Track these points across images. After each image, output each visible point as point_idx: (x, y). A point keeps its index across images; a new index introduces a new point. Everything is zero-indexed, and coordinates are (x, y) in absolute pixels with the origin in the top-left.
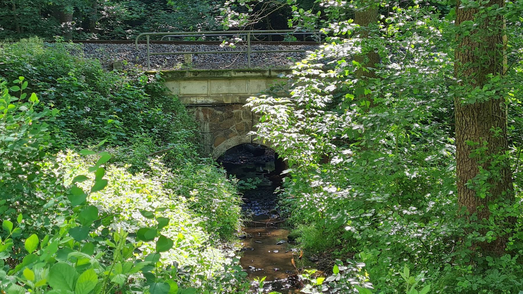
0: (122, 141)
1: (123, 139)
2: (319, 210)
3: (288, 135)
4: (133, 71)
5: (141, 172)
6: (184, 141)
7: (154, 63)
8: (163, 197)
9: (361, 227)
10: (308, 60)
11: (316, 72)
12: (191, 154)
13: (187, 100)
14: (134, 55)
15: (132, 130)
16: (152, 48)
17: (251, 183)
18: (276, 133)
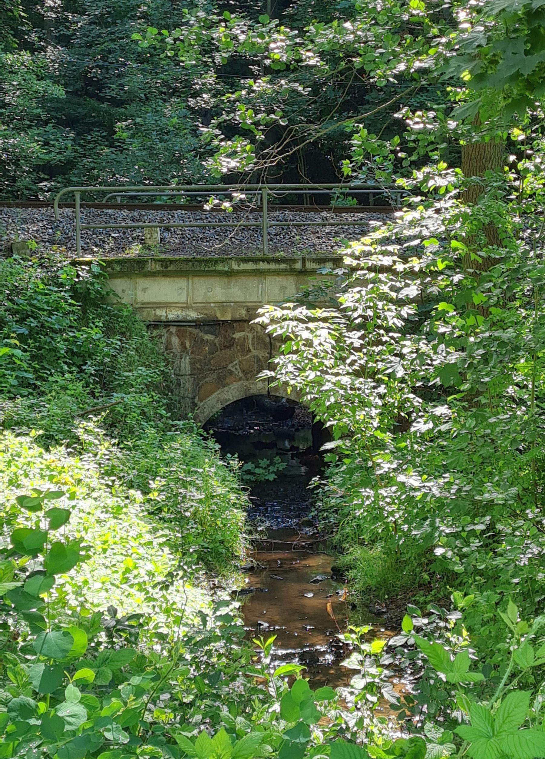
0: (27, 387)
1: (29, 385)
2: (389, 520)
3: (334, 379)
4: (48, 259)
5: (61, 445)
6: (143, 389)
7: (88, 243)
8: (101, 491)
9: (465, 550)
10: (372, 239)
11: (387, 261)
12: (157, 413)
13: (148, 313)
14: (52, 228)
15: (45, 369)
16: (86, 215)
17: (265, 468)
18: (312, 375)
